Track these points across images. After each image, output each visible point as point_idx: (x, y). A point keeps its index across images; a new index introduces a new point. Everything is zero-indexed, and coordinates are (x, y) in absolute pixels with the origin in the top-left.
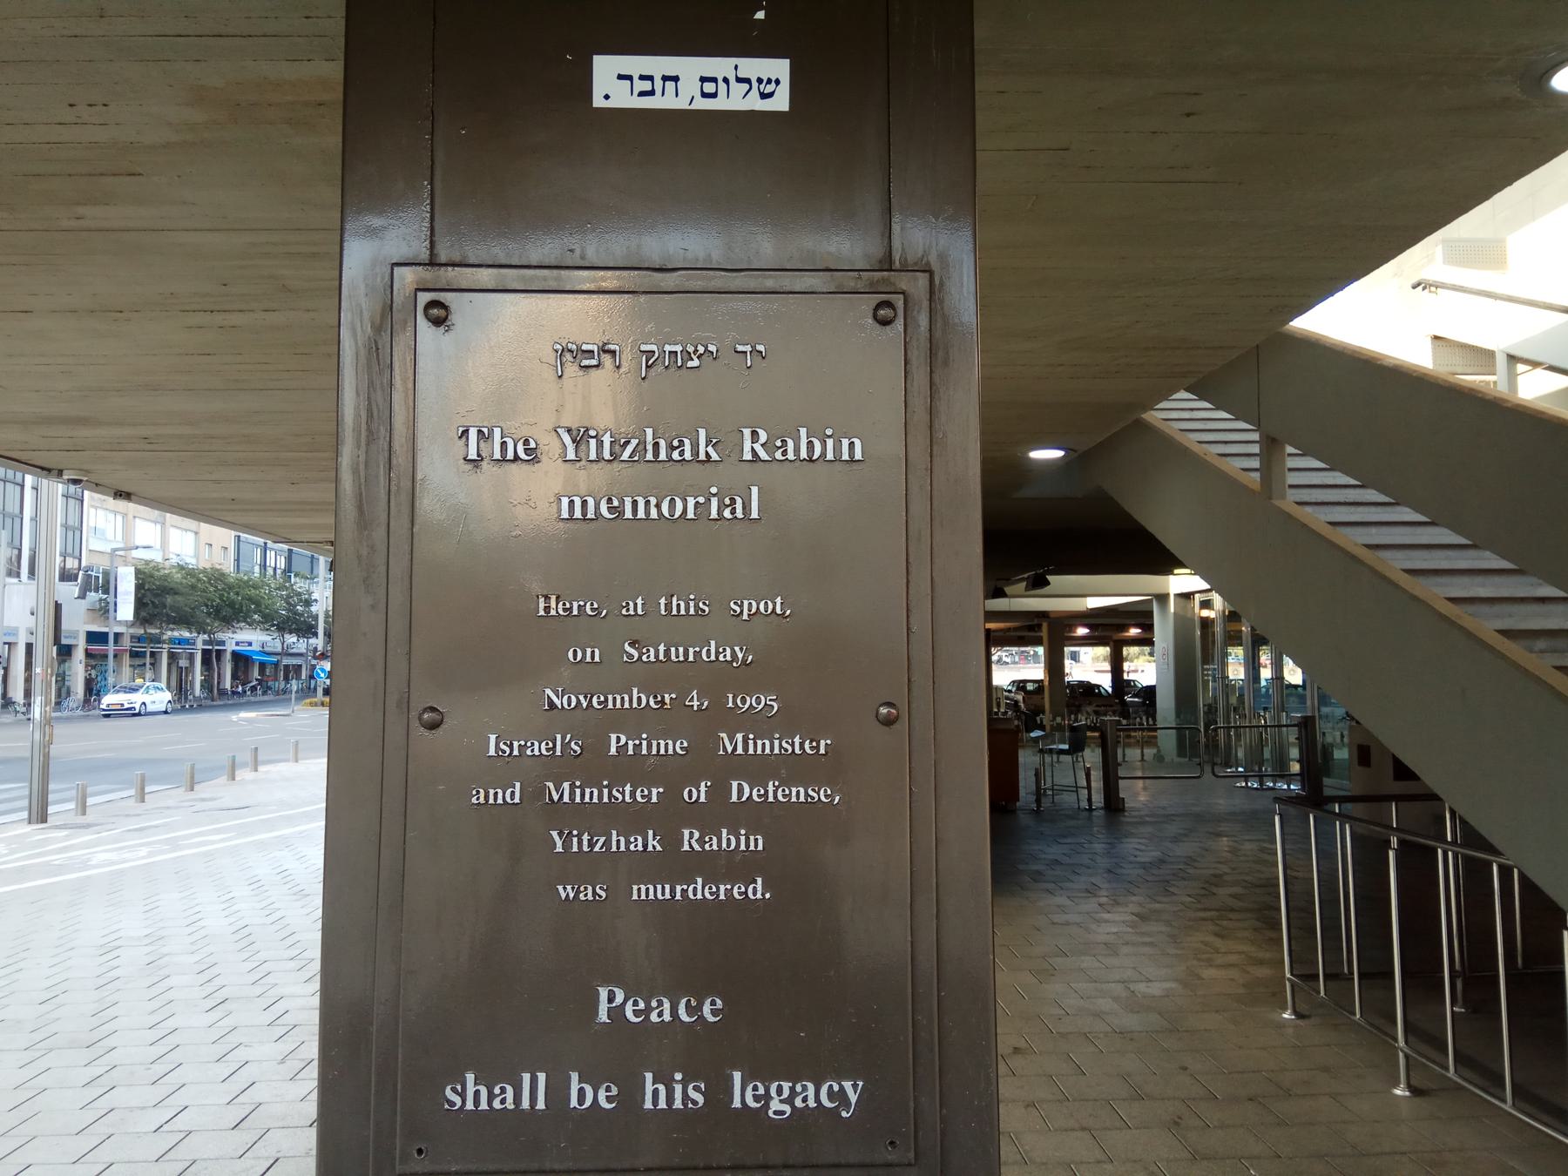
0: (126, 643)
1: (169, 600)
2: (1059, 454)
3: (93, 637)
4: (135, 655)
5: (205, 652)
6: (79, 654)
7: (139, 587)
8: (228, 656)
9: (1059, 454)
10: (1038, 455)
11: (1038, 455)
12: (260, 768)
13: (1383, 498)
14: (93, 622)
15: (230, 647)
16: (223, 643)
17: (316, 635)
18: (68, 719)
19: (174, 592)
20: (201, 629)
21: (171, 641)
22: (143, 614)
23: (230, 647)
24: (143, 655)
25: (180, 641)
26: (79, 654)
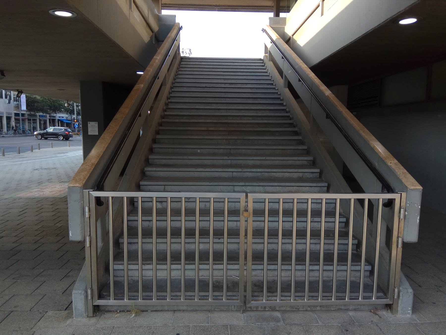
0: (26, 117)
1: (36, 104)
2: (138, 73)
3: (17, 115)
4: (29, 120)
5: (50, 119)
6: (13, 119)
7: (27, 101)
8: (57, 120)
9: (138, 73)
10: (59, 13)
11: (59, 13)
12: (34, 151)
13: (99, 250)
14: (16, 110)
15: (57, 118)
16: (55, 117)
17: (74, 114)
18: (9, 137)
19: (38, 102)
20: (47, 113)
21: (40, 116)
22: (29, 108)
23: (57, 118)
24: (30, 120)
25: (42, 116)
26: (13, 119)
